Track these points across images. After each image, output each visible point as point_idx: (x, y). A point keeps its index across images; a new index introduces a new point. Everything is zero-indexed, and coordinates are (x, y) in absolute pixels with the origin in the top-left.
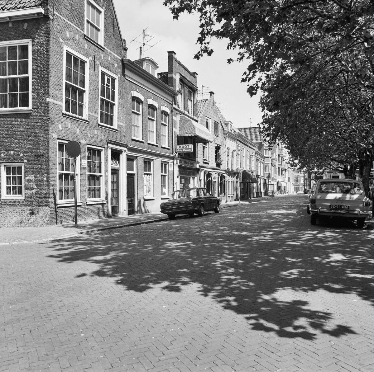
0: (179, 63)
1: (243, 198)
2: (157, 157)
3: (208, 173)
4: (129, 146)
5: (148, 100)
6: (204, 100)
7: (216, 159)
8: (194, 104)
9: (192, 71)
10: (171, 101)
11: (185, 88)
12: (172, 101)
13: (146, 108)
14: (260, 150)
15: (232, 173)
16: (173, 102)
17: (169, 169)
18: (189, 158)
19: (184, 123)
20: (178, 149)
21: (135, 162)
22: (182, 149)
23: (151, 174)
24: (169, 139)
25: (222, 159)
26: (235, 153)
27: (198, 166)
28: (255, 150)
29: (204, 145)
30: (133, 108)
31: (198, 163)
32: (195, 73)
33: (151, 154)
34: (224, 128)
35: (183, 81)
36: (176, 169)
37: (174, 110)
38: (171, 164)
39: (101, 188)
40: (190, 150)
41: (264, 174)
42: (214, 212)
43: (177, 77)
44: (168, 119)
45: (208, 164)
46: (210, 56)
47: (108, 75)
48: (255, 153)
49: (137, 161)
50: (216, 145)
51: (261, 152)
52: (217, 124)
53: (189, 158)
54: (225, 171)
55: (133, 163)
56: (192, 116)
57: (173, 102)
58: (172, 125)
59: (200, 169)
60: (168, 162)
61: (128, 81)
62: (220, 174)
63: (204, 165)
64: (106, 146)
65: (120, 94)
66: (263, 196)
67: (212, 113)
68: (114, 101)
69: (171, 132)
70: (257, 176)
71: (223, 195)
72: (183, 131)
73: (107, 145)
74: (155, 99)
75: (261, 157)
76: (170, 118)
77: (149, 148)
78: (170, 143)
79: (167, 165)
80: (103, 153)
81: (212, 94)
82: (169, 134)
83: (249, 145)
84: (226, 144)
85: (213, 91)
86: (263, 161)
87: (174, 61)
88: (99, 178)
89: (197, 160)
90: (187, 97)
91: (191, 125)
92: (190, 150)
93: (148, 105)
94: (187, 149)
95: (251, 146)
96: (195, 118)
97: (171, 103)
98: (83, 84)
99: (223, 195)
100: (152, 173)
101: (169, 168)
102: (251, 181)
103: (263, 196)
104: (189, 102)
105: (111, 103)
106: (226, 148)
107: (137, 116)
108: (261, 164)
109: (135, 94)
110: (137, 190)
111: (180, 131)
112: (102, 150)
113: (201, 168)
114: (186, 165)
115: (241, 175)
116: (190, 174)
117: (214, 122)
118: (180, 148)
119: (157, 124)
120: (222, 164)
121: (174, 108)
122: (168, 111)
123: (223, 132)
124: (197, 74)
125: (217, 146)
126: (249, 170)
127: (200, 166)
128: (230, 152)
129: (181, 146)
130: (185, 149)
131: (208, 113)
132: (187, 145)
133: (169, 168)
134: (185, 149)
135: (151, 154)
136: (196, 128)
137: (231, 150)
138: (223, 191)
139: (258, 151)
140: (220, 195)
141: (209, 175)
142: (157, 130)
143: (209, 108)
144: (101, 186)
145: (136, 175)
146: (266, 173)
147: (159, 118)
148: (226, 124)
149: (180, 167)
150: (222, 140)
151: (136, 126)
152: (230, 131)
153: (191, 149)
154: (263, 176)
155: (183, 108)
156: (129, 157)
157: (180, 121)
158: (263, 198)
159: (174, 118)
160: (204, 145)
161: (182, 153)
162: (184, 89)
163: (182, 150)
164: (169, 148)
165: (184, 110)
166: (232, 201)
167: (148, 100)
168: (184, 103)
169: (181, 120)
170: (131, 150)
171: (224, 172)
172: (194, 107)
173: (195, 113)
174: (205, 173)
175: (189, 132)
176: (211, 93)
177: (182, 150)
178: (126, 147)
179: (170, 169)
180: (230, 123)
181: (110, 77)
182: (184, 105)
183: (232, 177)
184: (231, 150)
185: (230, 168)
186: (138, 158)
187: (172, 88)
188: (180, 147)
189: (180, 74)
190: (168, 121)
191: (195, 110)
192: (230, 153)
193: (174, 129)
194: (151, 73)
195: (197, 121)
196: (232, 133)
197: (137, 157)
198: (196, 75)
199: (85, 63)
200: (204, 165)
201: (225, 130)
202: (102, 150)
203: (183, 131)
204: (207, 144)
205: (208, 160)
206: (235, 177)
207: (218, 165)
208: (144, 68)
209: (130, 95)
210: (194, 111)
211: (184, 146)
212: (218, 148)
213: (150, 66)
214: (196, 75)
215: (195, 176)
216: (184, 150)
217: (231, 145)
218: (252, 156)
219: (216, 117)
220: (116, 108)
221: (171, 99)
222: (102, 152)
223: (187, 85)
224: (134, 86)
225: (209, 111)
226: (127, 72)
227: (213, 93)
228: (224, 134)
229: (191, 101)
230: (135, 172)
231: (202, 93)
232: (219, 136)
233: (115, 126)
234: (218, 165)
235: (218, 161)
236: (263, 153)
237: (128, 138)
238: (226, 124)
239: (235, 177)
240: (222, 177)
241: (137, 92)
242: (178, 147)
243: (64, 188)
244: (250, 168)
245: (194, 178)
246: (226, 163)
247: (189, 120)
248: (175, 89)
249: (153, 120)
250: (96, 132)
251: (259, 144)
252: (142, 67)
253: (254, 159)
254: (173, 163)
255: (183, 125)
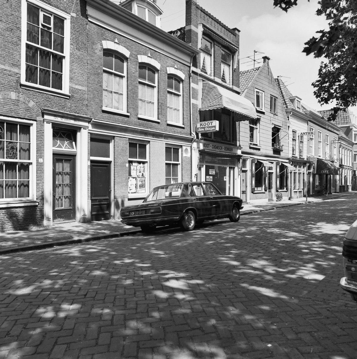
0: (203, 11)
1: (317, 194)
2: (156, 137)
3: (257, 161)
4: (93, 120)
5: (138, 56)
6: (256, 68)
7: (273, 145)
8: (233, 70)
9: (231, 27)
10: (188, 62)
11: (216, 47)
12: (190, 62)
13: (135, 69)
14: (347, 136)
15: (297, 162)
16: (190, 63)
17: (182, 156)
18: (222, 141)
19: (208, 91)
20: (198, 128)
21: (111, 145)
22: (204, 128)
23: (147, 162)
24: (183, 113)
25: (281, 144)
26: (305, 137)
27: (239, 152)
28: (338, 135)
29: (252, 126)
30: (171, 87)
31: (240, 147)
32: (235, 29)
33: (146, 133)
34: (288, 105)
35: (208, 34)
36: (196, 156)
37: (192, 74)
38: (186, 149)
39: (30, 182)
40: (214, 128)
41: (352, 164)
42: (228, 219)
43: (200, 30)
44: (183, 87)
45: (259, 149)
46: (304, 51)
47: (44, 10)
48: (339, 138)
49: (114, 142)
50: (273, 126)
51: (349, 138)
52: (275, 100)
53: (222, 141)
54: (288, 159)
55: (109, 145)
56: (231, 86)
57: (190, 63)
58: (190, 94)
59: (242, 156)
60: (181, 146)
61: (94, 26)
62: (279, 164)
63: (252, 151)
64: (40, 118)
65: (75, 41)
66: (350, 190)
67: (267, 84)
68: (63, 53)
69: (187, 104)
70: (341, 166)
71: (285, 190)
72: (206, 103)
73: (43, 117)
74: (154, 54)
75: (349, 144)
76: (186, 85)
77: (140, 125)
78: (185, 120)
79: (180, 150)
80: (33, 130)
81: (267, 60)
82: (183, 107)
83: (330, 128)
84: (290, 125)
85: (268, 56)
86: (351, 149)
87: (193, 7)
88: (25, 167)
89: (238, 145)
90: (219, 59)
91: (217, 94)
92: (214, 128)
93: (168, 74)
94: (210, 127)
95: (332, 130)
96: (235, 88)
97: (189, 65)
98: (60, 46)
99: (285, 190)
100: (147, 160)
101: (182, 154)
102: (329, 172)
103: (350, 190)
104: (224, 67)
105: (55, 56)
106: (291, 130)
107: (118, 78)
108: (348, 152)
109: (108, 45)
110: (114, 185)
111: (202, 103)
112: (32, 124)
113: (244, 155)
114: (217, 150)
115: (316, 165)
116: (225, 162)
117: (269, 96)
118: (202, 126)
119: (158, 92)
120: (282, 151)
121: (193, 72)
122: (182, 75)
123: (286, 110)
124: (239, 31)
125: (275, 127)
126: (328, 158)
127: (243, 153)
128: (297, 136)
129: (203, 123)
130: (208, 127)
131: (260, 84)
132: (210, 122)
133: (182, 154)
134: (208, 127)
135: (146, 133)
136: (223, 97)
137: (298, 133)
138: (285, 185)
139: (344, 136)
140: (279, 191)
141: (259, 165)
142: (158, 100)
143: (262, 78)
144: (30, 179)
145: (113, 163)
146: (354, 162)
147: (162, 84)
148: (292, 101)
149: (201, 153)
150: (283, 120)
151: (115, 93)
152: (297, 109)
153: (215, 127)
154: (351, 166)
155: (213, 74)
156: (93, 137)
157: (203, 89)
158: (351, 193)
159: (193, 85)
160: (252, 126)
161: (211, 133)
162: (214, 48)
163: (203, 129)
164: (183, 126)
165: (214, 76)
166: (300, 197)
167: (138, 56)
168: (214, 67)
169: (204, 88)
170: (97, 125)
171: (287, 161)
172: (233, 74)
173: (235, 82)
174: (252, 162)
175: (215, 104)
176: (266, 58)
177: (203, 129)
178: (89, 122)
179: (184, 155)
180: (297, 99)
181: (52, 15)
182: (214, 69)
183: (300, 167)
184: (298, 133)
185: (297, 155)
186: (115, 138)
187: (190, 44)
188: (201, 125)
189: (203, 25)
190: (183, 89)
191: (235, 78)
192: (297, 138)
193: (193, 101)
194: (147, 20)
195: (238, 93)
196: (301, 112)
197: (114, 137)
198: (237, 32)
199: (63, 21)
200: (252, 151)
201: (289, 107)
202: (32, 124)
203: (206, 103)
204: (258, 125)
205: (259, 145)
206: (306, 168)
207: (277, 151)
208: (133, 12)
209: (100, 46)
210: (233, 80)
211: (206, 123)
212: (276, 130)
213: (147, 10)
214: (237, 32)
215: (235, 165)
216: (207, 129)
217: (301, 127)
218: (333, 142)
219: (272, 90)
220: (66, 64)
221: (188, 59)
222: (31, 128)
223: (219, 43)
224: (107, 34)
225: (261, 81)
226: (90, 11)
227: (269, 59)
228: (287, 113)
229: (230, 66)
230: (111, 159)
231: (255, 61)
232: (278, 114)
233: (66, 90)
234: (277, 151)
235: (275, 146)
236: (352, 139)
237: (94, 107)
238: (292, 101)
239: (306, 168)
240: (283, 167)
241: (175, 68)
242: (198, 126)
243: (4, 182)
244: (331, 156)
245: (234, 168)
246: (291, 149)
247: (214, 87)
248: (197, 46)
249: (179, 95)
250: (13, 95)
251: (346, 128)
252: (131, 10)
253: (337, 145)
254: (191, 147)
255: (207, 94)
